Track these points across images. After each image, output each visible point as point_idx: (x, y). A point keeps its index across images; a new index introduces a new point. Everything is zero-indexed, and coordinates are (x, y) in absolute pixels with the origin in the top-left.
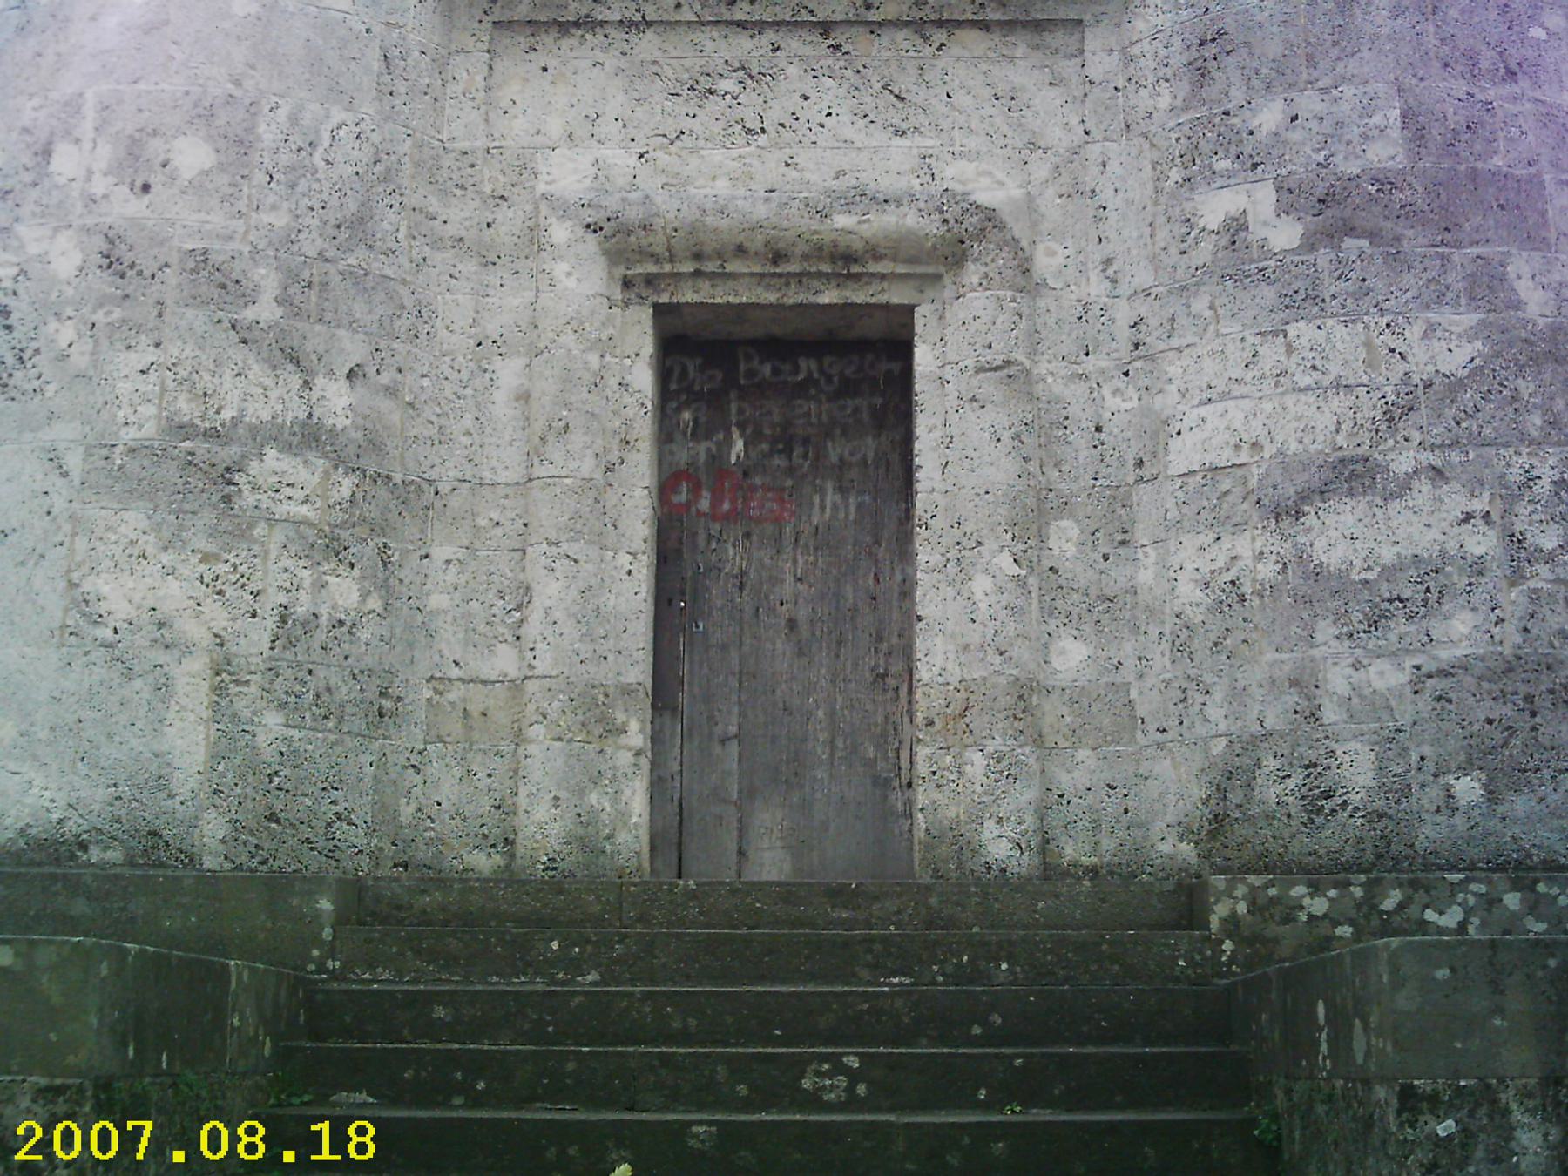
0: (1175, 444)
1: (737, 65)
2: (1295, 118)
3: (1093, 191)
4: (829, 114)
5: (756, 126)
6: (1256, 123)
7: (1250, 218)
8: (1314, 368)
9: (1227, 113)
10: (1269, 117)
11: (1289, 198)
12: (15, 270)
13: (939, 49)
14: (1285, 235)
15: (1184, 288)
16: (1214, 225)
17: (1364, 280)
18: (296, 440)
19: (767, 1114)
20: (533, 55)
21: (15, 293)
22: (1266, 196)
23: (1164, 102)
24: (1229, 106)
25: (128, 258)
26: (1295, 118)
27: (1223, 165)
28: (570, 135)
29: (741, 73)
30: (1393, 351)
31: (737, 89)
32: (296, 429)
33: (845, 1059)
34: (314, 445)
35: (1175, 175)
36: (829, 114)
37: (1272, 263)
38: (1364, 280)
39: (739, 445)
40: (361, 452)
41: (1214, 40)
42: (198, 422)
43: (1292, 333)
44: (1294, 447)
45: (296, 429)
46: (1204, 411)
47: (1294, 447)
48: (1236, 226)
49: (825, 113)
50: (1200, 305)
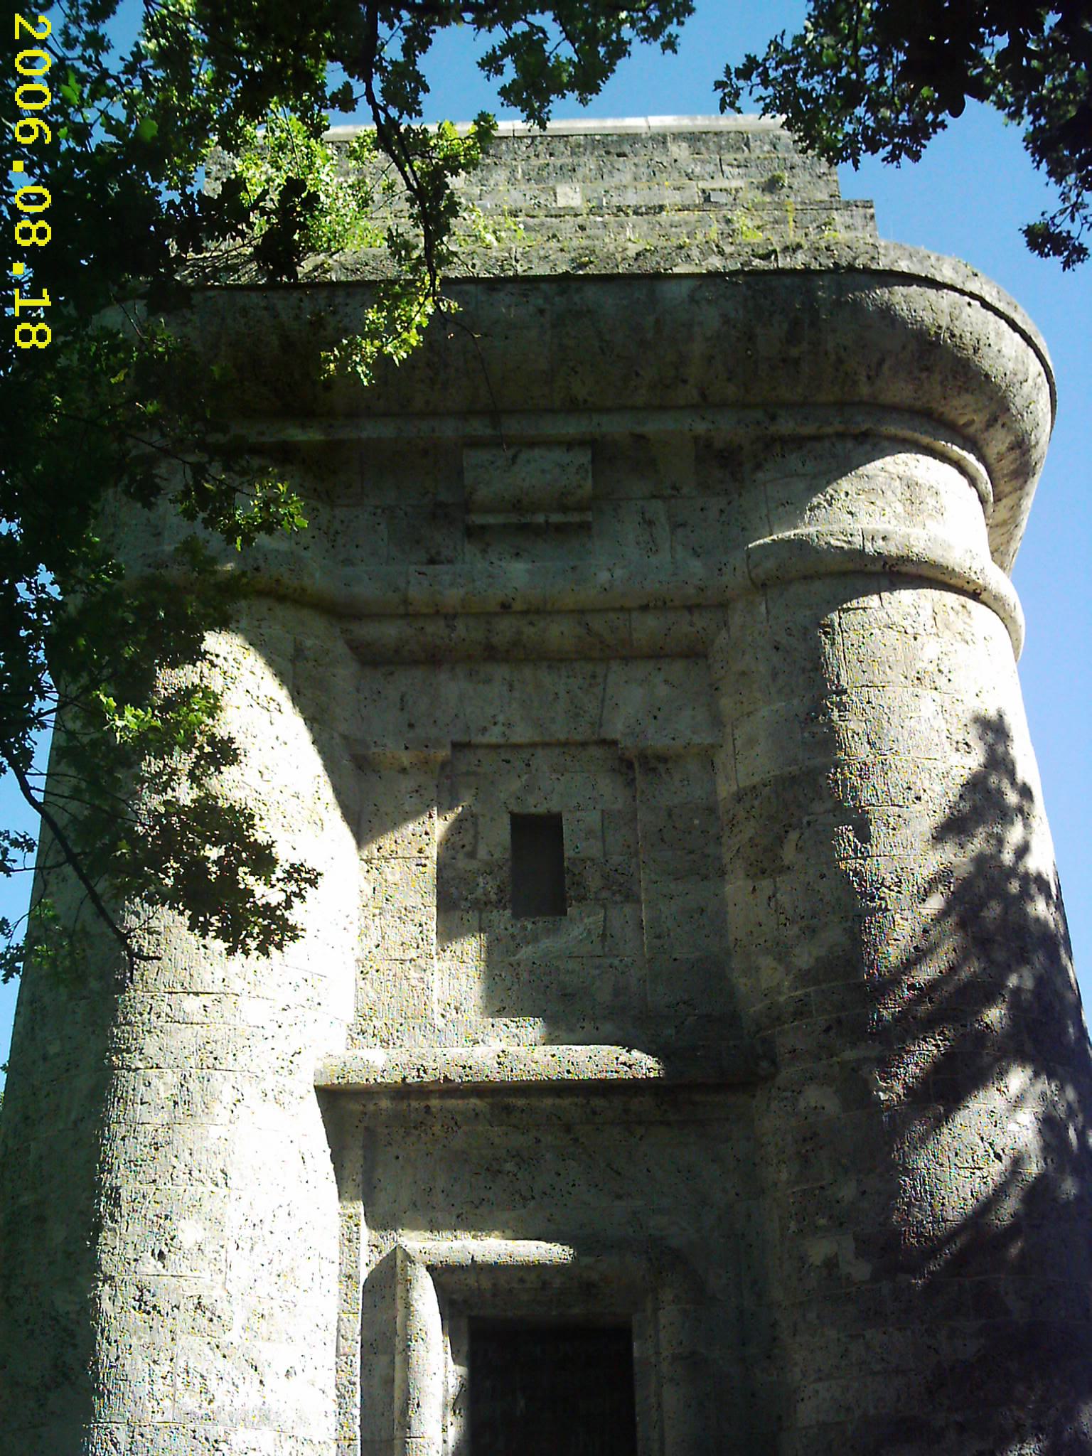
0: (801, 1406)
1: (514, 1153)
2: (864, 1193)
3: (743, 1235)
4: (574, 1185)
5: (528, 1195)
6: (840, 1195)
7: (840, 1258)
8: (883, 1359)
9: (822, 1188)
10: (847, 1192)
11: (864, 1247)
12: (78, 1307)
13: (640, 1139)
14: (861, 1271)
15: (801, 1303)
16: (818, 1263)
17: (910, 1301)
18: (256, 1420)
19: (303, 426)
20: (389, 1148)
21: (78, 1322)
22: (849, 1244)
23: (784, 1176)
24: (824, 1183)
25: (152, 1301)
26: (864, 1193)
27: (822, 1222)
28: (414, 1204)
29: (517, 1159)
30: (929, 1347)
31: (515, 1169)
32: (256, 1412)
33: (32, 791)
34: (267, 1422)
35: (793, 1226)
36: (574, 1185)
37: (854, 1289)
38: (910, 1301)
39: (522, 1403)
40: (294, 1425)
41: (811, 1139)
42: (197, 1410)
43: (868, 1336)
44: (872, 1411)
45: (256, 1412)
46: (819, 1386)
47: (872, 1411)
48: (831, 1264)
49: (571, 1184)
50: (812, 1316)
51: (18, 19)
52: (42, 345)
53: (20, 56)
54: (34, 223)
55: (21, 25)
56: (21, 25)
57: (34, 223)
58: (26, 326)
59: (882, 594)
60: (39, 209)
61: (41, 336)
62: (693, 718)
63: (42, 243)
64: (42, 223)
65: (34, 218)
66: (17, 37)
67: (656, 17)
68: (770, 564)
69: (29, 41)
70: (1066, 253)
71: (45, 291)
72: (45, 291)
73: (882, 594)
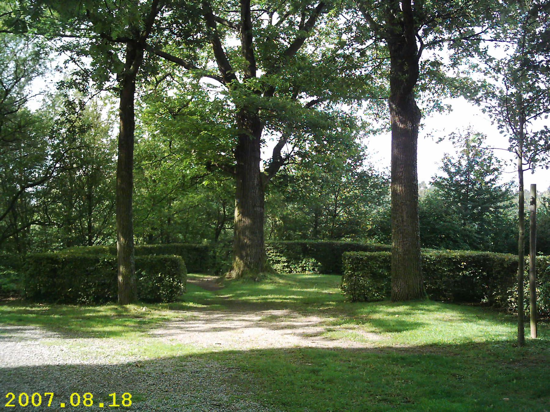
51: (7, 405)
52: (92, 396)
53: (21, 404)
54: (84, 399)
55: (10, 404)
56: (10, 404)
57: (84, 399)
58: (123, 402)
59: (523, 169)
60: (79, 398)
61: (127, 396)
62: (17, 86)
63: (130, 396)
64: (84, 396)
65: (82, 399)
66: (14, 406)
67: (14, 14)
68: (116, 60)
69: (16, 402)
70: (470, 28)
71: (110, 395)
72: (110, 395)
73: (523, 169)
